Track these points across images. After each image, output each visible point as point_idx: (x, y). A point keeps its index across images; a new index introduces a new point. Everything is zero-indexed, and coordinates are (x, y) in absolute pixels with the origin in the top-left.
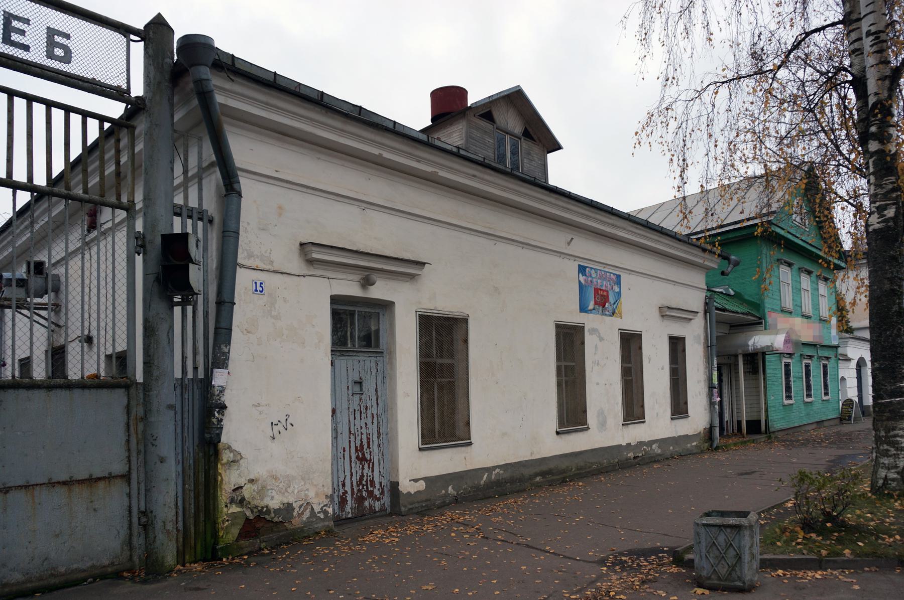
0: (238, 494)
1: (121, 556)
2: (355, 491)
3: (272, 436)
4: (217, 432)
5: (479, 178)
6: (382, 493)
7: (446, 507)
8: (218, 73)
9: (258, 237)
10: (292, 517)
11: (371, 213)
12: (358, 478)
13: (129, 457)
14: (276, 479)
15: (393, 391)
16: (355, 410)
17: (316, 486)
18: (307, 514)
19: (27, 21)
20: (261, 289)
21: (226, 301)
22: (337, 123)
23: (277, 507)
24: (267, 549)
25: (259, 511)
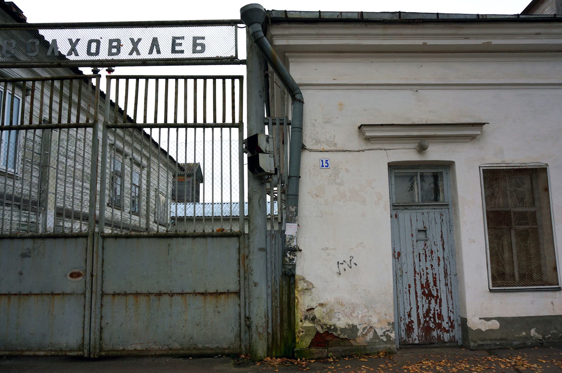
0: (310, 313)
1: (235, 344)
2: (422, 321)
3: (339, 272)
4: (289, 267)
5: (545, 34)
6: (452, 326)
7: (525, 349)
8: (278, 26)
9: (323, 129)
10: (357, 336)
11: (423, 93)
12: (425, 310)
13: (239, 281)
14: (342, 305)
15: (459, 237)
16: (420, 254)
17: (379, 314)
18: (370, 335)
19: (203, 38)
20: (327, 165)
21: (292, 176)
22: (378, 30)
23: (343, 327)
24: (332, 358)
25: (328, 327)
